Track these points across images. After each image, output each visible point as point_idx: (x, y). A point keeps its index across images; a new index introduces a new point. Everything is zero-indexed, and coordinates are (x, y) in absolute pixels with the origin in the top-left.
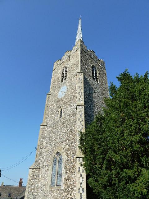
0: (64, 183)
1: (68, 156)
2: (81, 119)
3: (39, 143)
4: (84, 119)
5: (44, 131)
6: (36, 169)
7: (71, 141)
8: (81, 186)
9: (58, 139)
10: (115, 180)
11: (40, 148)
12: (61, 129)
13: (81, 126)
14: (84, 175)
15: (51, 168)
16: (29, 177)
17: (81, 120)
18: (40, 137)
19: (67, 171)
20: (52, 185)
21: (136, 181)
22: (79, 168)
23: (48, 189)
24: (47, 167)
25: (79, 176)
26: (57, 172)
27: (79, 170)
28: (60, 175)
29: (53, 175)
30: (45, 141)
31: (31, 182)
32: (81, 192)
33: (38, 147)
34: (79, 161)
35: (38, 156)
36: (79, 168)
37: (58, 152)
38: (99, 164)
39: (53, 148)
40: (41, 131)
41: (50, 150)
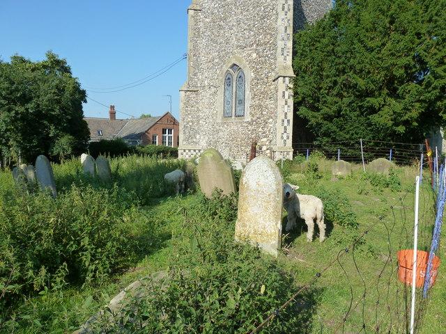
0: (251, 113)
1: (256, 71)
2: (286, 6)
3: (190, 45)
4: (292, 7)
5: (196, 22)
6: (191, 91)
7: (263, 47)
8: (286, 117)
9: (234, 41)
10: (346, 110)
11: (194, 55)
12: (239, 22)
13: (286, 20)
14: (291, 102)
15: (221, 90)
16: (182, 104)
17: (286, 10)
18: (190, 33)
19: (255, 95)
20: (226, 116)
21: (380, 112)
22: (284, 92)
23: (219, 121)
24: (213, 89)
25: (284, 103)
26: (234, 97)
27: (284, 96)
28: (241, 102)
29: (226, 102)
30: (203, 42)
31: (186, 111)
32: (286, 124)
33: (189, 52)
34: (284, 82)
35: (192, 70)
36: (284, 92)
37: (235, 65)
38: (326, 89)
39: (224, 56)
40: (191, 22)
41: (216, 60)
